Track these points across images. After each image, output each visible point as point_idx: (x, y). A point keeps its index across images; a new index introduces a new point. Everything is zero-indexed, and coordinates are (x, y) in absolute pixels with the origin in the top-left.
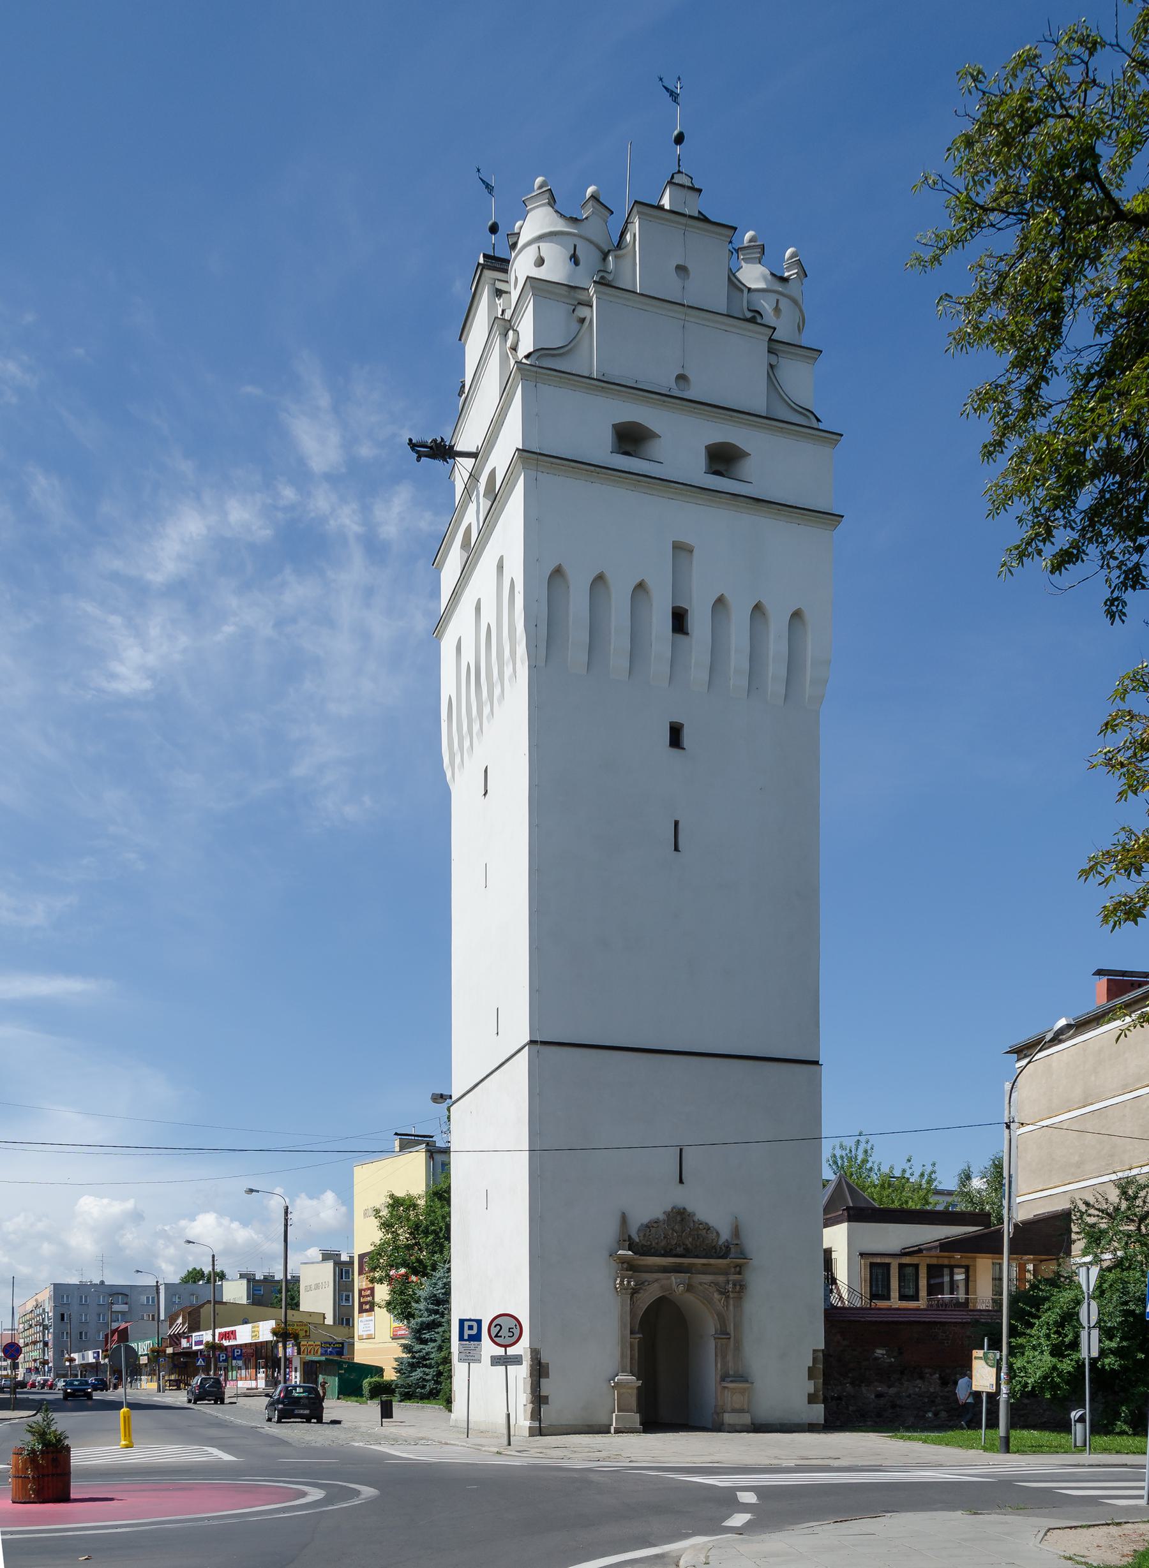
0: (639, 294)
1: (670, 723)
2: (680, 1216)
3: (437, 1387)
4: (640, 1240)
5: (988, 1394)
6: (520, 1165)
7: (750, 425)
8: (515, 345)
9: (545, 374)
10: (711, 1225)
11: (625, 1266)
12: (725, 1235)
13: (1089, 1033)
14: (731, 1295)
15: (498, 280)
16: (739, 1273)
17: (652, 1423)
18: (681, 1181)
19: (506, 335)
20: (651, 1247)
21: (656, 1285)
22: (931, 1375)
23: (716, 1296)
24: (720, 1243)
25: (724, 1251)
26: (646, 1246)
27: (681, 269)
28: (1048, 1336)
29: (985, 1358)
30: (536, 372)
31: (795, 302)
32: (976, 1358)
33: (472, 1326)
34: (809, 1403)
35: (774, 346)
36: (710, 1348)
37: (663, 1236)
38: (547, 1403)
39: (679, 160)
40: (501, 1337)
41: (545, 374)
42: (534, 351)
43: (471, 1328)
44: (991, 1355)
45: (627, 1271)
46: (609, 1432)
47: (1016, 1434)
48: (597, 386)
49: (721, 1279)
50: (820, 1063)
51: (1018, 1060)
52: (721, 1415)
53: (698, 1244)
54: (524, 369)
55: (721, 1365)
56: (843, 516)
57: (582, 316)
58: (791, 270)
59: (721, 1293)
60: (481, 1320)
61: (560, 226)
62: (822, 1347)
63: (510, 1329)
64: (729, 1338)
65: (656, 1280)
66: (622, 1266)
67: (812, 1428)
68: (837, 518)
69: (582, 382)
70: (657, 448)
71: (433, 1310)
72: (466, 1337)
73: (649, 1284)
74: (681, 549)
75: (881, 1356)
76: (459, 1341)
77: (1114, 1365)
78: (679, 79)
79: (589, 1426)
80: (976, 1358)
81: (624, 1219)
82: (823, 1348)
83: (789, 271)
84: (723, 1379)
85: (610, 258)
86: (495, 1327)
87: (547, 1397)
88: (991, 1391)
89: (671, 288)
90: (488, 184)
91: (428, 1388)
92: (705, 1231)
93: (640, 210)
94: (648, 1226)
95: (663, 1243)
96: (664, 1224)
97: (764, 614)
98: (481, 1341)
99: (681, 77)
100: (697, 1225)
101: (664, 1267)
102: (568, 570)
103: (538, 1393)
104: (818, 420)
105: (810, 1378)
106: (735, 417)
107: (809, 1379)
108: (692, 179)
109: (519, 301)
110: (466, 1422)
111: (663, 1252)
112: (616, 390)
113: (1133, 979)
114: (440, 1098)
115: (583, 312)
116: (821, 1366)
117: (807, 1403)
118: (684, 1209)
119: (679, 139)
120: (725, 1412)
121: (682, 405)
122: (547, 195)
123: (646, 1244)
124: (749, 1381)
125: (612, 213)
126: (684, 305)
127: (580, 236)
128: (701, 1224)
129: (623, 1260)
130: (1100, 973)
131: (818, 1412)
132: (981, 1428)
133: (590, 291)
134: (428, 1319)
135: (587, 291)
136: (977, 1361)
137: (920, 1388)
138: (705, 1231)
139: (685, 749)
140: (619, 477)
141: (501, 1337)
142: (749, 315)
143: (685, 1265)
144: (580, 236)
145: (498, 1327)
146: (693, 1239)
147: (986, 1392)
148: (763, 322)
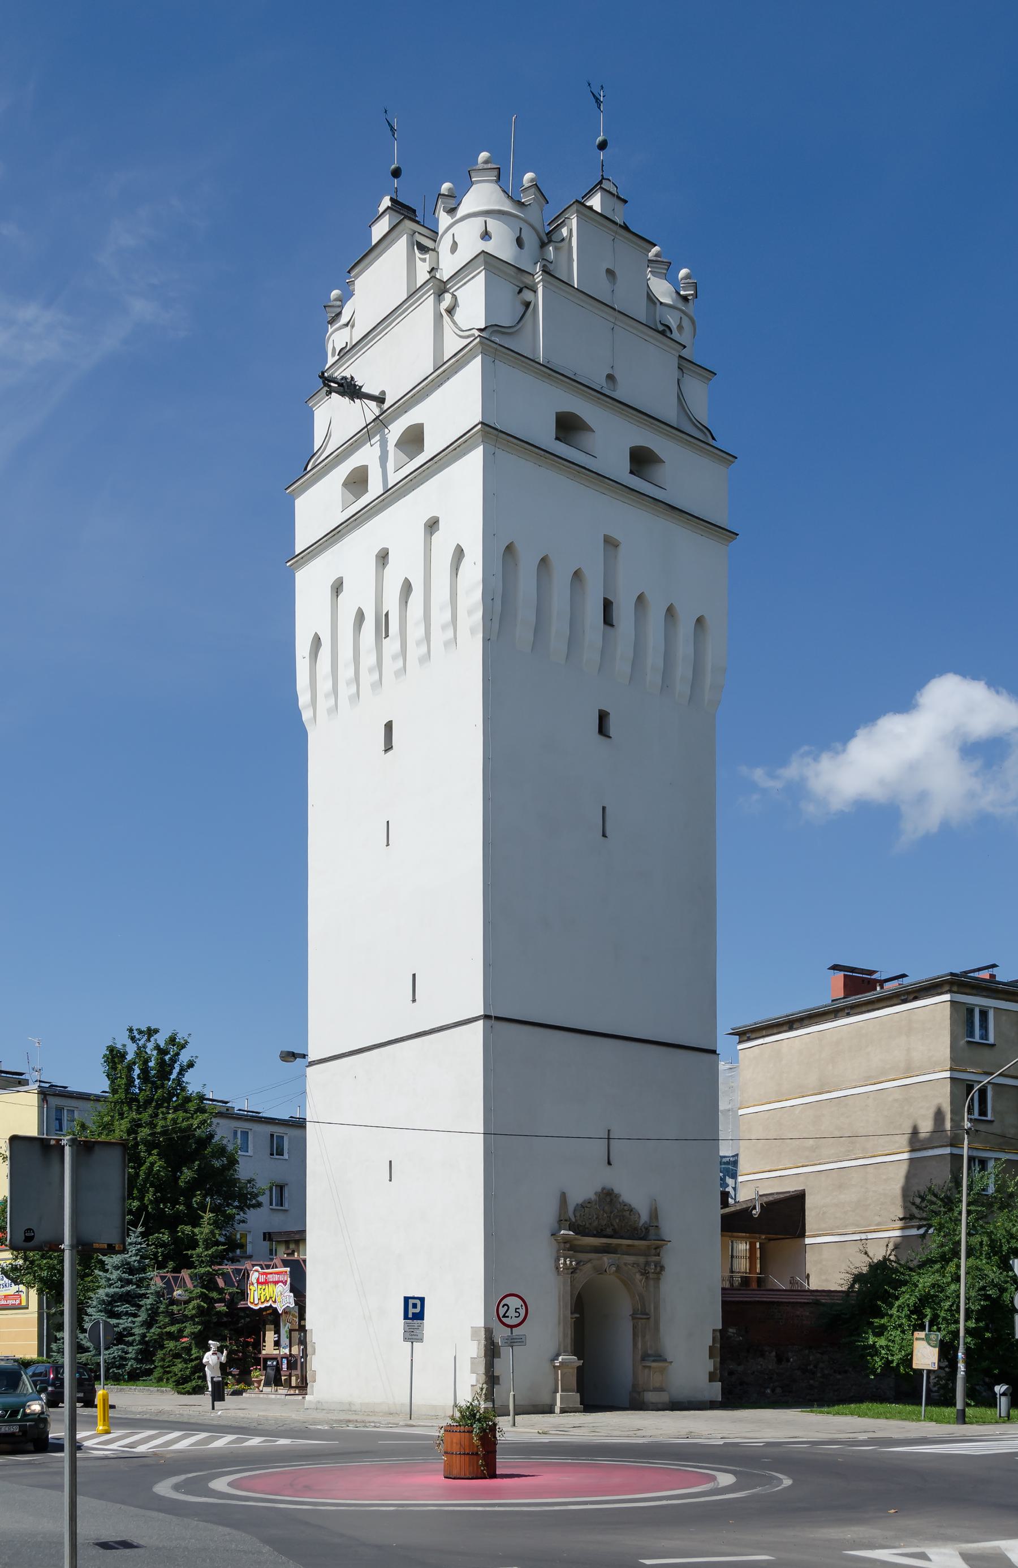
0: (577, 289)
1: (599, 710)
2: (608, 1196)
3: (141, 1367)
4: (576, 1220)
5: (929, 1372)
6: (477, 1143)
7: (668, 435)
8: (452, 307)
9: (504, 353)
10: (633, 1206)
11: (568, 1246)
12: (644, 1218)
13: (823, 1025)
14: (651, 1276)
15: (419, 233)
16: (659, 1256)
17: (591, 1404)
18: (609, 1163)
19: (439, 296)
20: (586, 1226)
21: (589, 1265)
22: (770, 1353)
23: (638, 1276)
24: (641, 1224)
25: (644, 1233)
26: (581, 1226)
27: (610, 273)
28: (908, 1317)
29: (927, 1339)
30: (496, 349)
31: (693, 322)
32: (917, 1339)
33: (416, 1304)
34: (710, 1381)
35: (684, 364)
36: (625, 1329)
37: (595, 1216)
38: (499, 1384)
39: (603, 165)
40: (508, 1317)
41: (504, 353)
42: (486, 328)
43: (415, 1306)
44: (933, 1336)
45: (568, 1251)
46: (551, 1411)
47: (969, 1411)
48: (545, 372)
49: (641, 1260)
50: (717, 1053)
51: (740, 1042)
53: (623, 1225)
54: (486, 344)
55: (641, 1345)
56: (737, 535)
57: (528, 300)
58: (688, 291)
59: (642, 1274)
61: (507, 206)
62: (720, 1327)
63: (516, 1309)
64: (648, 1319)
65: (590, 1260)
66: (564, 1246)
67: (712, 1405)
68: (732, 535)
70: (586, 440)
71: (127, 1279)
72: (410, 1316)
73: (583, 1264)
74: (611, 543)
75: (732, 1335)
76: (404, 1319)
77: (970, 1344)
78: (602, 86)
79: (534, 1406)
80: (917, 1339)
81: (563, 1198)
82: (721, 1328)
83: (685, 291)
84: (643, 1359)
85: (551, 248)
86: (503, 1307)
87: (498, 1377)
88: (933, 1369)
89: (601, 289)
90: (392, 127)
91: (128, 1368)
92: (628, 1212)
93: (578, 209)
94: (583, 1206)
95: (596, 1223)
96: (596, 1204)
97: (673, 616)
98: (423, 1320)
99: (603, 86)
100: (622, 1207)
101: (595, 1247)
102: (519, 547)
103: (491, 1373)
104: (713, 438)
105: (710, 1357)
106: (655, 425)
107: (710, 1358)
108: (617, 188)
109: (465, 269)
111: (595, 1232)
113: (864, 976)
114: (290, 1056)
115: (528, 295)
116: (719, 1346)
118: (612, 1190)
119: (603, 146)
120: (644, 1391)
121: (613, 405)
122: (495, 173)
123: (581, 1224)
124: (668, 1361)
125: (548, 203)
126: (614, 309)
127: (526, 221)
128: (625, 1205)
129: (566, 1240)
130: (835, 968)
132: (921, 1404)
133: (535, 277)
134: (123, 1289)
135: (532, 276)
136: (918, 1341)
137: (761, 1365)
138: (628, 1212)
139: (610, 737)
141: (508, 1317)
142: (661, 328)
143: (613, 1245)
144: (526, 221)
145: (506, 1307)
146: (620, 1220)
147: (927, 1370)
148: (671, 336)
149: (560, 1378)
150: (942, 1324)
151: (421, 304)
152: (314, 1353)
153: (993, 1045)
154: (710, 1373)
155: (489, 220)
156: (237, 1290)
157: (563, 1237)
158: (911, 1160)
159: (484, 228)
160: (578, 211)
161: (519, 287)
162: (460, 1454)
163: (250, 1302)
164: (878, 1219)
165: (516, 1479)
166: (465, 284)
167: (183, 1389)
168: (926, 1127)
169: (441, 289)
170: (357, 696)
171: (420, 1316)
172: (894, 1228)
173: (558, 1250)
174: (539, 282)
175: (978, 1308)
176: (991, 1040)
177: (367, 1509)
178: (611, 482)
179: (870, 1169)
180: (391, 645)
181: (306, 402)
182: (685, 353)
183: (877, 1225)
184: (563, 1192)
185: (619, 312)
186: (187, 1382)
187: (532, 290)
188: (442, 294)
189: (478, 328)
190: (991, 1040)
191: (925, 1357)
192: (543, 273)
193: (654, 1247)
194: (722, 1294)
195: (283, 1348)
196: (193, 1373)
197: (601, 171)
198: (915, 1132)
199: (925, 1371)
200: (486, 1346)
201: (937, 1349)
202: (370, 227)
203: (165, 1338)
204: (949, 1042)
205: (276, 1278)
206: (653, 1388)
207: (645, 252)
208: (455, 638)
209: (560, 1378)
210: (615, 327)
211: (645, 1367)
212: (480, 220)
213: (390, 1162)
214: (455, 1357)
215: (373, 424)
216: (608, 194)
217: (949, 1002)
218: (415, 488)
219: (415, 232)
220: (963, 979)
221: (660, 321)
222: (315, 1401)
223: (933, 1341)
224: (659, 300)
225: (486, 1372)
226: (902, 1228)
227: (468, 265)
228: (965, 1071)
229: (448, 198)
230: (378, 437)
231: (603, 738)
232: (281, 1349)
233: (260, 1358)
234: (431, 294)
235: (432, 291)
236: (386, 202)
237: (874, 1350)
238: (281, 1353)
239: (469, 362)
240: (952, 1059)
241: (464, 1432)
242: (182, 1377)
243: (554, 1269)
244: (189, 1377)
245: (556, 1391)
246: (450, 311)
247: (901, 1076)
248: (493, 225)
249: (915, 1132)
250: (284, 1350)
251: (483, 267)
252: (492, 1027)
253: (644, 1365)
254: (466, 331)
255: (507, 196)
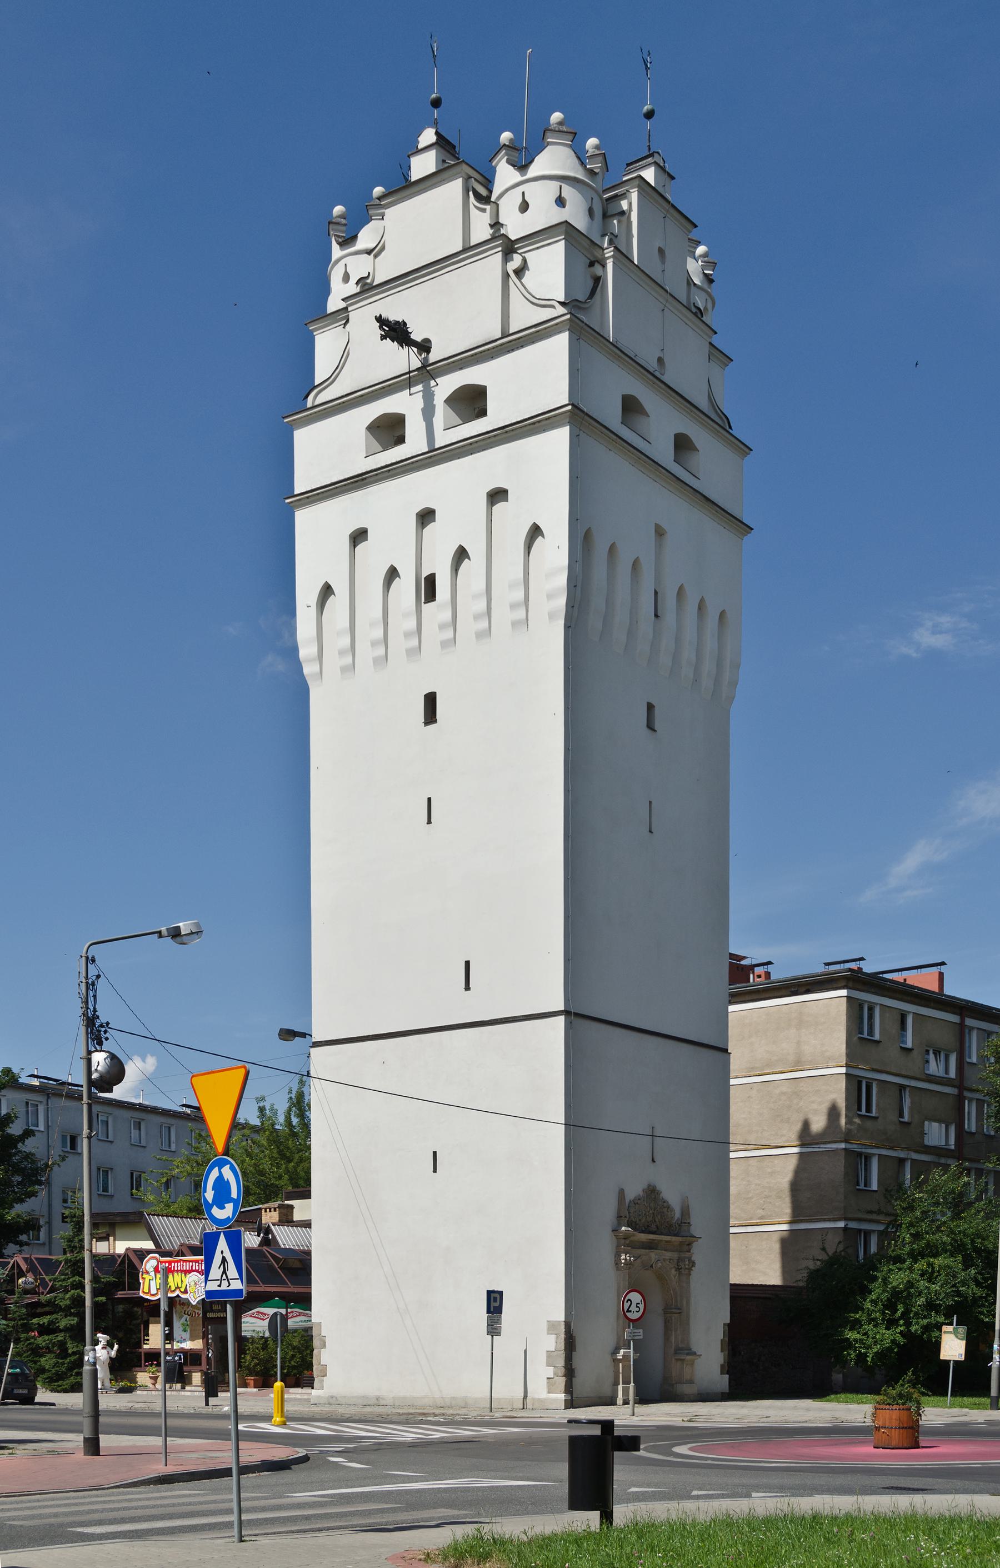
2: (652, 1192)
5: (955, 1362)
15: (475, 179)
18: (653, 1161)
23: (673, 1272)
27: (661, 251)
29: (955, 1333)
30: (582, 328)
32: (945, 1332)
40: (630, 1311)
43: (495, 1300)
50: (729, 1052)
52: (675, 1386)
60: (502, 1292)
61: (580, 175)
69: (610, 349)
72: (492, 1310)
79: (600, 1398)
81: (621, 1193)
82: (729, 1322)
85: (615, 222)
86: (627, 1302)
89: (653, 269)
94: (635, 1202)
98: (501, 1314)
104: (730, 427)
110: (489, 1400)
112: (627, 362)
114: (288, 1034)
115: (598, 270)
117: (720, 1373)
119: (649, 115)
120: (676, 1383)
121: (666, 392)
122: (601, 158)
124: (697, 1354)
125: (608, 171)
126: (666, 291)
128: (664, 1202)
129: (626, 1236)
131: (723, 1382)
132: (947, 1395)
138: (666, 1209)
140: (629, 451)
141: (630, 1311)
147: (953, 1361)
149: (621, 1371)
150: (913, 1318)
151: (484, 258)
152: (324, 1346)
153: (878, 1042)
154: (721, 1365)
155: (563, 185)
156: (114, 1279)
157: (625, 1233)
158: (801, 1154)
159: (559, 194)
160: (639, 186)
161: (589, 259)
162: (899, 1428)
163: (143, 1292)
164: (760, 1212)
165: (935, 1448)
166: (538, 248)
167: (59, 1386)
168: (818, 1124)
169: (509, 248)
170: (385, 658)
171: (499, 1310)
172: (779, 1221)
173: (618, 1246)
174: (609, 258)
175: (952, 1304)
176: (877, 1037)
177: (956, 1466)
178: (663, 471)
179: (751, 1161)
180: (436, 612)
181: (306, 324)
182: (716, 340)
183: (761, 1218)
184: (622, 1189)
185: (671, 295)
186: (63, 1379)
187: (601, 264)
188: (509, 253)
189: (560, 301)
190: (877, 1037)
191: (952, 1348)
192: (615, 250)
193: (687, 1243)
194: (731, 1289)
195: (178, 1342)
196: (70, 1369)
197: (647, 141)
198: (806, 1125)
199: (952, 1362)
200: (565, 1339)
201: (964, 1342)
202: (409, 156)
203: (20, 1330)
204: (845, 1038)
205: (187, 1266)
206: (686, 1381)
207: (687, 232)
208: (527, 620)
209: (621, 1371)
210: (666, 309)
211: (677, 1360)
212: (555, 185)
213: (435, 1153)
214: (525, 1352)
215: (416, 372)
216: (660, 169)
217: (846, 998)
218: (474, 453)
219: (470, 177)
220: (859, 975)
221: (694, 303)
222: (327, 1396)
223: (961, 1334)
224: (693, 281)
225: (565, 1365)
226: (790, 1223)
227: (544, 231)
228: (857, 1068)
229: (514, 150)
230: (420, 387)
231: (650, 731)
232: (175, 1343)
233: (141, 1352)
234: (499, 252)
235: (500, 249)
236: (428, 136)
237: (848, 1344)
238: (175, 1348)
239: (551, 336)
240: (848, 1055)
241: (903, 1409)
242: (57, 1373)
243: (613, 1264)
244: (66, 1374)
245: (617, 1384)
246: (519, 272)
247: (790, 1069)
248: (568, 192)
249: (806, 1125)
250: (179, 1344)
251: (563, 237)
252: (571, 1023)
253: (676, 1358)
254: (539, 299)
255: (580, 163)
